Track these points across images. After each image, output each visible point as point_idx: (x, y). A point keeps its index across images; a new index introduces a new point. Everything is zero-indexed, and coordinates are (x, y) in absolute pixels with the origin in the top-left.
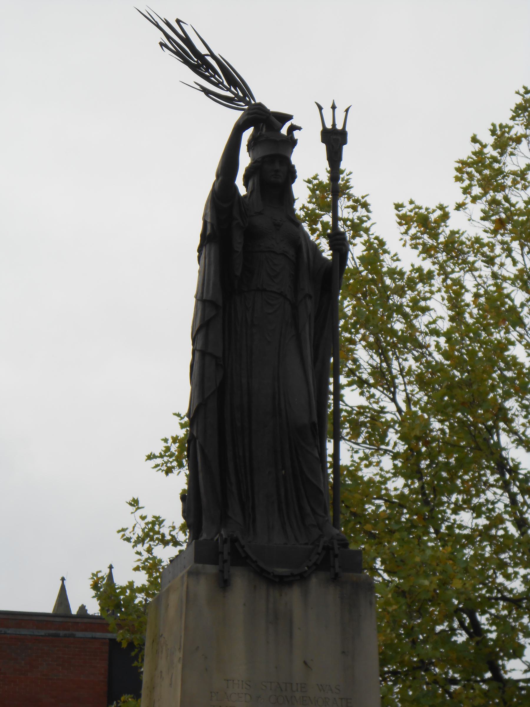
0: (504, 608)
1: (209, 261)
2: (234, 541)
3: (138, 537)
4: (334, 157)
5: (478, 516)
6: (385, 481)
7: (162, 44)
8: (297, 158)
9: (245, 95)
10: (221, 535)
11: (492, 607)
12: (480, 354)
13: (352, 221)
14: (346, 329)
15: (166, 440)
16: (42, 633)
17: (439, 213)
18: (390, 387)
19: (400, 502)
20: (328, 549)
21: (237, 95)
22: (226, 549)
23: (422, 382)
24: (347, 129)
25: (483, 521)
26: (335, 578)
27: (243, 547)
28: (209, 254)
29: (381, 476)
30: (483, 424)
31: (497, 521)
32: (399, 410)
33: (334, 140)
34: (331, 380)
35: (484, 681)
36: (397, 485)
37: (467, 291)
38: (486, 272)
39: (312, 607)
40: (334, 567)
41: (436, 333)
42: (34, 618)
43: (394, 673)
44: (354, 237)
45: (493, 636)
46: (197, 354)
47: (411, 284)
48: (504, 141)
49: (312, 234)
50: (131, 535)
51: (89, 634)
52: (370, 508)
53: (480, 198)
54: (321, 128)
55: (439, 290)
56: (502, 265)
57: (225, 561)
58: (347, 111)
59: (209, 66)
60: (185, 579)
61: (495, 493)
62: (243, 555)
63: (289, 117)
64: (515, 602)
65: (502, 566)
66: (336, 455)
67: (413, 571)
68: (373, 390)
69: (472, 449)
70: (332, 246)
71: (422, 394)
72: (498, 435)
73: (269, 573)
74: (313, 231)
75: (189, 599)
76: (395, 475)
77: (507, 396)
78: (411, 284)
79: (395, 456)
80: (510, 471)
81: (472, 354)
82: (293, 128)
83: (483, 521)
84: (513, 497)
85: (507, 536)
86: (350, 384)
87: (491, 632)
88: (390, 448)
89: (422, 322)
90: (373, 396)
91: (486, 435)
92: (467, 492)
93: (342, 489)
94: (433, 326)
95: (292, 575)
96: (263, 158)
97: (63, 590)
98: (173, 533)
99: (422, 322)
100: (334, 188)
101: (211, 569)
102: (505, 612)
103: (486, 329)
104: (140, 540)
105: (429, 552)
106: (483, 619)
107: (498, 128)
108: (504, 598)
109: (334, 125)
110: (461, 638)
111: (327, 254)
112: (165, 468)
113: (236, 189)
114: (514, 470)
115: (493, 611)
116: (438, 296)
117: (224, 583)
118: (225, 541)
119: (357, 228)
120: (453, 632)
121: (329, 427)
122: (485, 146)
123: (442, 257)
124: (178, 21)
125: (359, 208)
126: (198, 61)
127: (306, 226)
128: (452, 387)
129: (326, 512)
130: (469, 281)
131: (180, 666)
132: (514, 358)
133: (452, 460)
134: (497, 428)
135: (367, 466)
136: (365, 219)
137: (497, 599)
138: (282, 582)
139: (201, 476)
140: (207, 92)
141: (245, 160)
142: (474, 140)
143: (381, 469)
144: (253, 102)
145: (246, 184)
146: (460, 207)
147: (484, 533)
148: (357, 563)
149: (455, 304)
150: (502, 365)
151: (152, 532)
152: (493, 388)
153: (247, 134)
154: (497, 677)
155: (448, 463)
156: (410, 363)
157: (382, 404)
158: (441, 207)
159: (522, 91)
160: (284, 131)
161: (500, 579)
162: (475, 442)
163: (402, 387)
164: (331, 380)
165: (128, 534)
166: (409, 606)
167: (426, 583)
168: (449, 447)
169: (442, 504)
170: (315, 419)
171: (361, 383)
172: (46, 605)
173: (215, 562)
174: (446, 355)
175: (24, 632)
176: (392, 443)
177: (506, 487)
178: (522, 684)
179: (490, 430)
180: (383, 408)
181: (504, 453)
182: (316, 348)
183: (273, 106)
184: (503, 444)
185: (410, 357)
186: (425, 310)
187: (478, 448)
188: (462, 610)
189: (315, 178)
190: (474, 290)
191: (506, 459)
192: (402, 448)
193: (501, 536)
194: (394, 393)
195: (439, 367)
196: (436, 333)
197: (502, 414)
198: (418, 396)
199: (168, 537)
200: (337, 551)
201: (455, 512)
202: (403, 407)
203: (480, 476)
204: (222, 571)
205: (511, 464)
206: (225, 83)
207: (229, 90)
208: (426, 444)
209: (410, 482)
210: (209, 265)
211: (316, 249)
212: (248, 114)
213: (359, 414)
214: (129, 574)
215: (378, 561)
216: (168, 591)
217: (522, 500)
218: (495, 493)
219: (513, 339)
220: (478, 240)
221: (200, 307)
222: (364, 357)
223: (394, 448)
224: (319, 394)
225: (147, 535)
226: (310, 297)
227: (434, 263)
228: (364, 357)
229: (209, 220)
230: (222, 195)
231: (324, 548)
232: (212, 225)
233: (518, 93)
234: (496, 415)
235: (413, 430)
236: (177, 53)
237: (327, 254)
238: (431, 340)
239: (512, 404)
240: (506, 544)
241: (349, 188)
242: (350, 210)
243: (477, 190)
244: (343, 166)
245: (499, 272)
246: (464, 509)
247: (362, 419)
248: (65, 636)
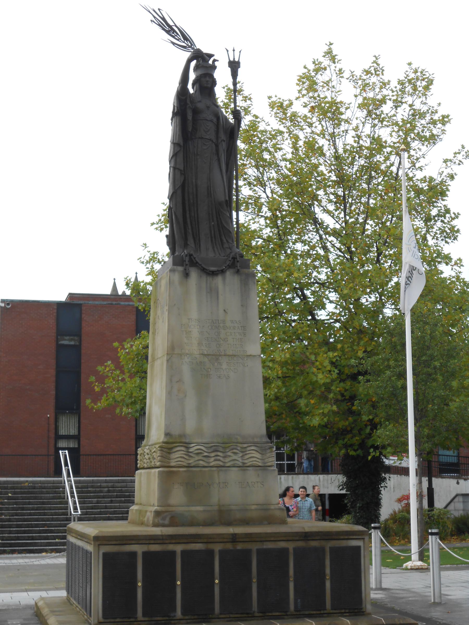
0: (317, 287)
1: (176, 124)
2: (191, 255)
3: (147, 261)
4: (234, 74)
5: (305, 245)
6: (261, 230)
7: (151, 21)
8: (217, 75)
9: (192, 45)
10: (185, 253)
11: (312, 287)
12: (305, 170)
13: (244, 107)
14: (241, 159)
15: (159, 216)
16: (105, 303)
17: (287, 102)
18: (263, 185)
19: (268, 240)
20: (234, 258)
21: (188, 45)
22: (187, 259)
23: (278, 183)
24: (240, 61)
25: (307, 247)
26: (238, 272)
27: (195, 258)
28: (176, 121)
29: (260, 228)
30: (307, 202)
31: (313, 248)
32: (268, 197)
33: (234, 66)
34: (235, 181)
35: (308, 320)
36: (267, 232)
37: (300, 140)
38: (308, 130)
39: (227, 285)
40: (237, 266)
41: (285, 160)
42: (101, 297)
43: (267, 317)
44: (245, 115)
45: (312, 300)
46: (172, 169)
47: (274, 137)
48: (319, 69)
49: (226, 113)
50: (144, 260)
51: (127, 303)
52: (254, 243)
53: (306, 95)
54: (228, 61)
55: (287, 139)
56: (316, 127)
57: (187, 265)
58: (240, 52)
59: (174, 31)
60: (168, 273)
61: (312, 235)
62: (195, 262)
63: (212, 55)
64: (322, 285)
65: (315, 267)
66: (237, 218)
67: (275, 270)
68: (255, 188)
69: (302, 214)
70: (235, 117)
71: (279, 189)
72: (314, 208)
73: (207, 270)
74: (227, 112)
75: (171, 282)
76: (266, 227)
77: (318, 189)
78: (274, 137)
79: (266, 218)
80: (319, 224)
81: (302, 169)
82: (215, 61)
83: (307, 247)
84: (321, 237)
85: (318, 254)
86: (245, 185)
87: (311, 298)
88: (263, 214)
89: (278, 155)
90: (255, 190)
91: (308, 208)
92: (299, 234)
93: (240, 234)
94: (284, 157)
95: (218, 271)
96: (201, 75)
97: (115, 284)
98: (163, 258)
99: (278, 155)
100: (235, 91)
101: (180, 268)
102: (318, 289)
103: (308, 157)
104: (148, 262)
105: (282, 261)
106: (308, 293)
107: (316, 61)
108: (318, 283)
109: (234, 59)
110: (297, 301)
111: (232, 121)
112: (159, 229)
113: (188, 90)
114: (321, 224)
115: (313, 289)
116: (286, 142)
117: (186, 275)
118: (186, 256)
119: (247, 111)
120: (294, 298)
121: (234, 205)
122: (309, 71)
123: (289, 124)
124: (159, 9)
125: (248, 100)
126: (170, 29)
127: (223, 110)
128: (292, 185)
129: (233, 241)
130: (301, 135)
131: (167, 313)
132: (322, 171)
133: (293, 220)
134: (314, 204)
135: (253, 223)
136: (250, 106)
137: (314, 283)
138: (213, 274)
139: (174, 225)
140: (174, 44)
141: (192, 76)
142: (305, 67)
143: (260, 225)
144: (195, 48)
145: (193, 88)
146: (297, 99)
147: (307, 254)
148: (246, 264)
149: (295, 147)
150: (316, 175)
151: (153, 258)
152: (311, 185)
153: (193, 63)
154: (314, 318)
155: (290, 221)
156: (273, 174)
157: (259, 194)
158: (290, 100)
159: (328, 44)
160: (210, 62)
161: (315, 274)
162: (303, 211)
163: (269, 186)
164: (235, 181)
165: (142, 260)
166: (273, 286)
167: (281, 275)
168: (291, 213)
169: (288, 240)
170: (227, 198)
171: (250, 184)
172: (107, 291)
173: (182, 265)
174: (289, 170)
175: (97, 303)
176: (264, 212)
177: (317, 232)
178: (326, 321)
179: (310, 205)
180: (260, 196)
181: (317, 216)
182: (227, 165)
183: (205, 50)
184: (316, 212)
185: (273, 171)
186: (280, 149)
187: (304, 214)
188: (297, 289)
189: (227, 86)
190: (304, 139)
191: (317, 219)
192: (269, 214)
193: (315, 254)
194: (265, 189)
195: (288, 176)
196: (285, 160)
197: (315, 197)
198: (277, 190)
199: (161, 260)
200: (238, 259)
201: (294, 243)
202: (270, 195)
203: (306, 226)
204: (185, 269)
205: (320, 221)
206: (182, 39)
207: (184, 42)
208: (280, 212)
209: (273, 230)
210: (176, 126)
211: (226, 119)
212: (193, 54)
213: (249, 199)
214: (145, 278)
215: (259, 266)
216: (161, 279)
217: (325, 237)
218: (312, 235)
219: (321, 163)
220: (305, 116)
221: (172, 146)
222: (252, 172)
223: (265, 214)
224: (229, 188)
225: (151, 260)
226: (224, 141)
227: (284, 127)
228: (252, 172)
229: (176, 105)
230: (182, 93)
231: (232, 258)
232: (177, 107)
233: (326, 44)
234: (313, 198)
235: (274, 206)
236: (159, 25)
237: (232, 121)
238: (283, 164)
239: (321, 192)
240: (318, 257)
241: (242, 91)
242: (244, 102)
243: (304, 92)
244: (238, 79)
245: (314, 130)
246: (298, 242)
247: (250, 201)
248: (116, 304)
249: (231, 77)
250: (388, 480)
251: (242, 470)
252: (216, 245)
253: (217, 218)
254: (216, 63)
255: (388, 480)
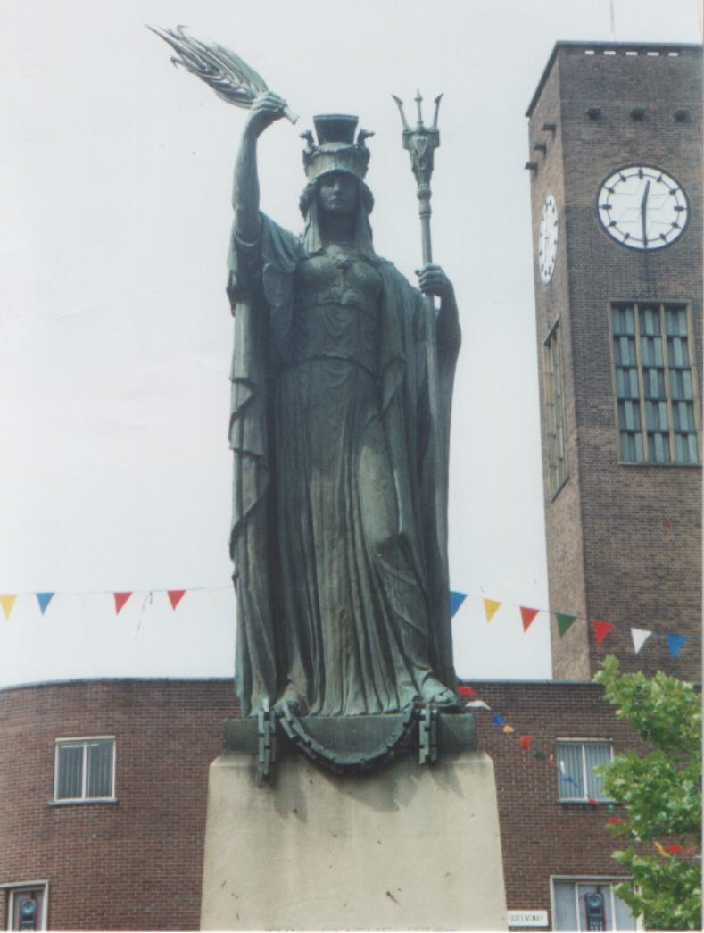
7: (174, 61)
24: (440, 127)
54: (401, 129)
58: (438, 101)
82: (363, 135)
230: (252, 234)
249: (412, 176)
250: (597, 129)
251: (402, 695)
252: (371, 675)
253: (373, 591)
254: (368, 143)
255: (597, 129)
